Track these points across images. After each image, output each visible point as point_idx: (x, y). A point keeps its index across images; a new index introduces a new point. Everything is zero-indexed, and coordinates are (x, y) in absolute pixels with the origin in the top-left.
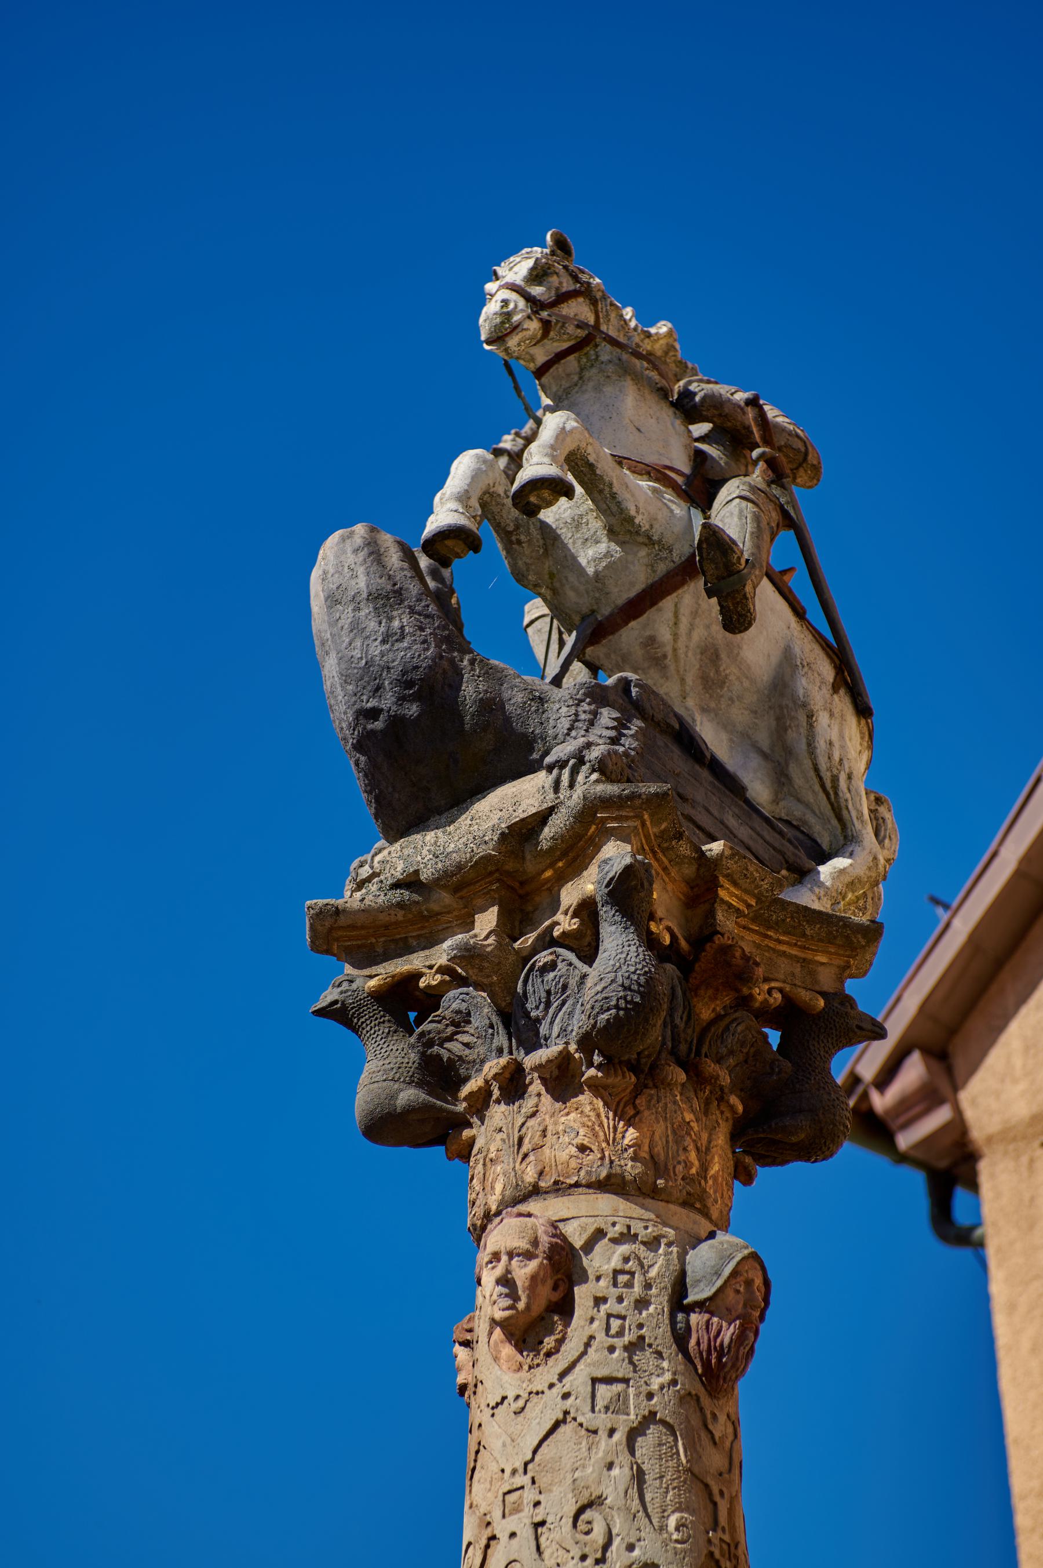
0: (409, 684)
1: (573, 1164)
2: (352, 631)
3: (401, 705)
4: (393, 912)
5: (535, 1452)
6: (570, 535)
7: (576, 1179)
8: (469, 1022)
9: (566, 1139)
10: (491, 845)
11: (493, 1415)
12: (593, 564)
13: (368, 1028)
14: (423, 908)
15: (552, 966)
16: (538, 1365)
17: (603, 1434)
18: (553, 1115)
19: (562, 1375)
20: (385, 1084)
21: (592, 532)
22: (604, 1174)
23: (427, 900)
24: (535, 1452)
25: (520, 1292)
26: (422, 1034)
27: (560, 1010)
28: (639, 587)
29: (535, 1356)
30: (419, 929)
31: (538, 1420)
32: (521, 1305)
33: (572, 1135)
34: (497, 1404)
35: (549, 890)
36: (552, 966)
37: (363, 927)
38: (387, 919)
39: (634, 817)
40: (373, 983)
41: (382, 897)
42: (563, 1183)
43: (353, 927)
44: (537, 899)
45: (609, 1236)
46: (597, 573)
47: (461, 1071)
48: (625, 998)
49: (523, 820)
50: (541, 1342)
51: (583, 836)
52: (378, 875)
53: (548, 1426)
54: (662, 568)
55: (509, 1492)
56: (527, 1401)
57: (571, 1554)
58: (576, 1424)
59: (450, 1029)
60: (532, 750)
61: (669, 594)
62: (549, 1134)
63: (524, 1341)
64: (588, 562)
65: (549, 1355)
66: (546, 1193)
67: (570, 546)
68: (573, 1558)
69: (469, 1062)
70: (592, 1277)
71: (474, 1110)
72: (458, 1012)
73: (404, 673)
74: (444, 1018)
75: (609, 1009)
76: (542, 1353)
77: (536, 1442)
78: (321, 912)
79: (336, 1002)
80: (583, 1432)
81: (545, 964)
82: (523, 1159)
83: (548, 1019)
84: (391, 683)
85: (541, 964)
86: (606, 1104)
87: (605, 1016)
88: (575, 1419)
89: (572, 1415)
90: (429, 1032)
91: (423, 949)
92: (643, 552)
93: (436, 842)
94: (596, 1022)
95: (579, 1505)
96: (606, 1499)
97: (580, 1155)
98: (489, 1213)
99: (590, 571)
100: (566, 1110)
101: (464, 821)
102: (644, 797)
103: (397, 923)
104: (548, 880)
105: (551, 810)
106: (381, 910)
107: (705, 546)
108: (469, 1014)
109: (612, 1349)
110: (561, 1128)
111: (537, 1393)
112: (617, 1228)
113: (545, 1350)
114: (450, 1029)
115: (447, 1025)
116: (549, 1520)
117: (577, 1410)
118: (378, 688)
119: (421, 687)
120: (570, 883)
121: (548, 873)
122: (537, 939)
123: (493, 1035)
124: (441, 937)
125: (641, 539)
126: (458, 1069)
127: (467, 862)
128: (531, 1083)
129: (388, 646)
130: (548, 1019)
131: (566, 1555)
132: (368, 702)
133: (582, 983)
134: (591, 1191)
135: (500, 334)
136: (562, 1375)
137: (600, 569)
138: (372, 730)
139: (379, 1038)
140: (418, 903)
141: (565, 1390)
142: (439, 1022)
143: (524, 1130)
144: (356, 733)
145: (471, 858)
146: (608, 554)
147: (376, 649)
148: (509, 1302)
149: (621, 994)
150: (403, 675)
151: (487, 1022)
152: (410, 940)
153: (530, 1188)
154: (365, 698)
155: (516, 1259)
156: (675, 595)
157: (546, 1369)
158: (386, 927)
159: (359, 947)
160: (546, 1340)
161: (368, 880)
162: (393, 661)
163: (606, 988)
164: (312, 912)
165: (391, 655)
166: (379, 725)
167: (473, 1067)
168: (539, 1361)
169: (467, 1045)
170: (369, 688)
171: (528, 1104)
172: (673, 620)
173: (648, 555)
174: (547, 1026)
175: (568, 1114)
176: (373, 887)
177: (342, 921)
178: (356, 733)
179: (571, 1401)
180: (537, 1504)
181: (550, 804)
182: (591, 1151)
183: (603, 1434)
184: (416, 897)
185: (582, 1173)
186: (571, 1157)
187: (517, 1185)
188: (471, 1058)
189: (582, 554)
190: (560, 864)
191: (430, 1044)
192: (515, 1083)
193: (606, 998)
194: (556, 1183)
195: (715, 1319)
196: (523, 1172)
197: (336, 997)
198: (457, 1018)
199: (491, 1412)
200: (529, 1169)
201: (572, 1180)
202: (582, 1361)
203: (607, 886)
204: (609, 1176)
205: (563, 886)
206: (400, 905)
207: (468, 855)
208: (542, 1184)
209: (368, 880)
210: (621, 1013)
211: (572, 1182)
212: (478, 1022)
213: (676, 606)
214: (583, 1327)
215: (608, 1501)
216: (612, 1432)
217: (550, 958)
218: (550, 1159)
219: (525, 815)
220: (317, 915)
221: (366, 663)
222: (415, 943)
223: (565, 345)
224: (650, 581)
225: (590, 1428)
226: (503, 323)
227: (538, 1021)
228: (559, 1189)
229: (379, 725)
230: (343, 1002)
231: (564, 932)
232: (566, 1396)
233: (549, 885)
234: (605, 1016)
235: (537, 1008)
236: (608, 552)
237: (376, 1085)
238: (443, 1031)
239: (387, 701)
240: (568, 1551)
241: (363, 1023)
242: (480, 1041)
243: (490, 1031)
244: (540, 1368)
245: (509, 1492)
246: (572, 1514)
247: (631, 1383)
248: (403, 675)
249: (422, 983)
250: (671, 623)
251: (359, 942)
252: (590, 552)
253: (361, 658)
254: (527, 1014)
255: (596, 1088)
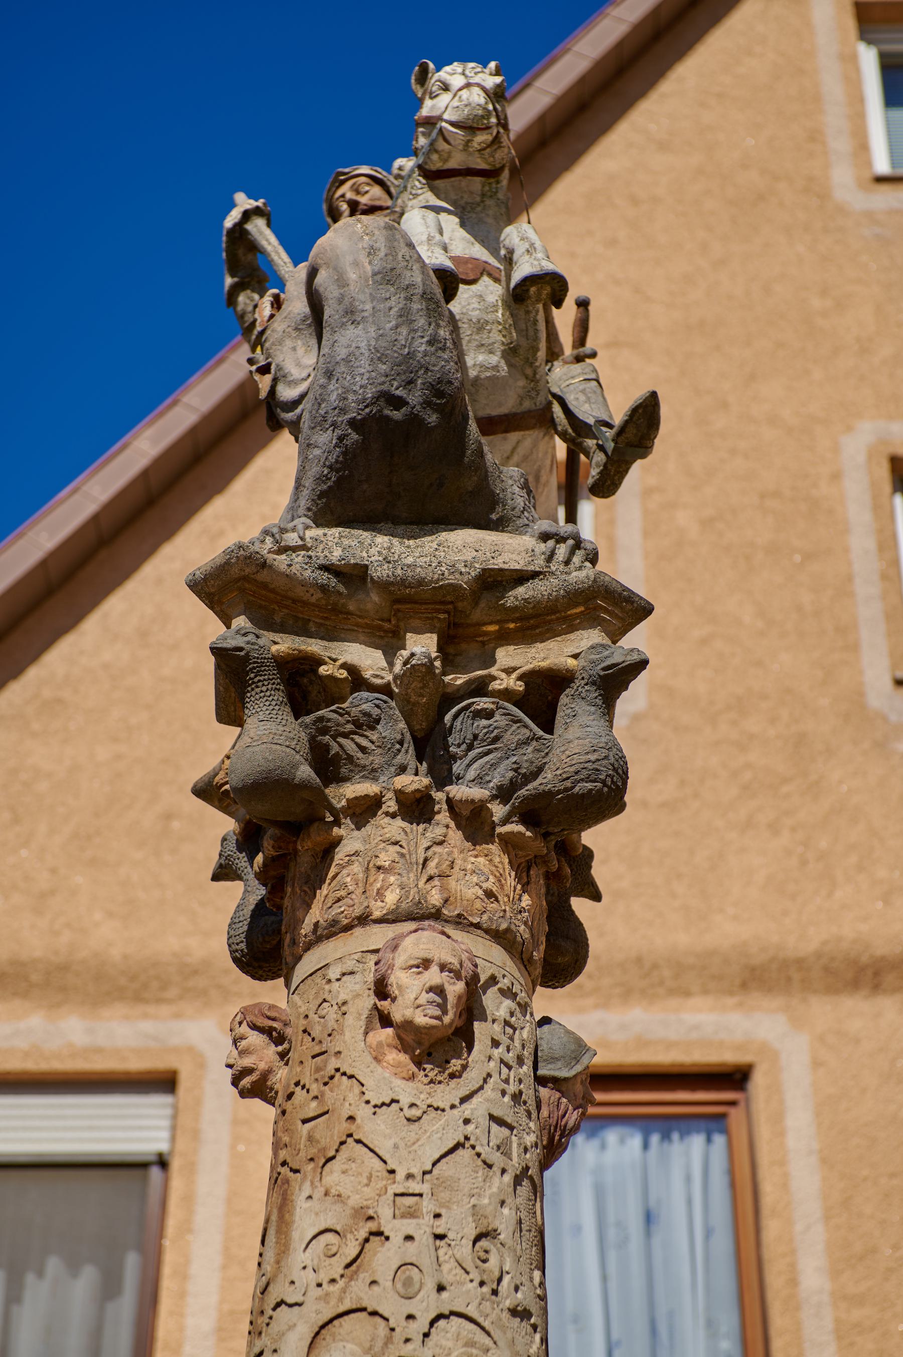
0: (440, 394)
1: (478, 905)
2: (401, 316)
3: (424, 408)
4: (312, 591)
5: (434, 1165)
6: (469, 333)
7: (478, 920)
8: (373, 728)
9: (475, 879)
10: (466, 578)
11: (374, 1113)
12: (478, 369)
13: (264, 688)
14: (344, 601)
15: (489, 715)
16: (440, 1082)
17: (496, 1170)
18: (462, 852)
19: (464, 1100)
20: (288, 750)
21: (491, 341)
22: (504, 926)
23: (350, 596)
24: (434, 1165)
25: (449, 1007)
26: (321, 719)
27: (482, 757)
28: (503, 410)
29: (440, 1072)
30: (323, 618)
31: (439, 1135)
32: (447, 1019)
33: (482, 878)
34: (383, 1104)
35: (483, 643)
36: (489, 715)
37: (273, 591)
38: (302, 594)
39: (622, 618)
40: (274, 648)
41: (309, 571)
42: (465, 918)
43: (264, 586)
44: (464, 646)
45: (499, 985)
46: (477, 378)
47: (343, 770)
48: (612, 777)
49: (501, 570)
50: (448, 1062)
51: (559, 612)
52: (308, 549)
53: (451, 1145)
54: (527, 405)
55: (402, 1195)
56: (424, 1112)
57: (471, 1276)
58: (473, 1152)
59: (350, 727)
60: (493, 510)
61: (520, 430)
62: (457, 868)
63: (429, 1054)
64: (474, 365)
65: (452, 1076)
66: (446, 921)
67: (464, 342)
68: (472, 1281)
69: (358, 765)
70: (490, 1019)
71: (350, 812)
72: (367, 714)
73: (440, 381)
74: (348, 713)
75: (595, 781)
76: (447, 1072)
77: (437, 1156)
78: (250, 557)
79: (241, 649)
80: (479, 1162)
81: (482, 710)
82: (428, 880)
83: (467, 761)
84: (424, 384)
85: (479, 707)
86: (510, 862)
87: (589, 785)
88: (473, 1147)
89: (472, 1142)
90: (329, 720)
91: (322, 638)
92: (522, 383)
93: (389, 548)
94: (573, 787)
95: (478, 1231)
96: (499, 1234)
97: (486, 900)
98: (368, 916)
99: (472, 373)
100: (475, 853)
101: (429, 543)
102: (635, 605)
103: (305, 603)
104: (486, 634)
105: (535, 575)
106: (303, 583)
107: (640, 411)
108: (378, 721)
109: (504, 1093)
110: (469, 866)
111: (437, 1109)
112: (506, 981)
113: (451, 1070)
114: (350, 727)
115: (348, 722)
116: (451, 1235)
117: (477, 1139)
118: (410, 382)
119: (448, 402)
120: (512, 647)
121: (492, 628)
122: (468, 683)
123: (399, 751)
124: (342, 635)
125: (529, 371)
126: (341, 767)
127: (431, 582)
128: (439, 812)
129: (433, 349)
130: (467, 761)
131: (465, 1275)
132: (397, 389)
133: (525, 743)
134: (487, 937)
135: (475, 125)
136: (464, 1100)
137: (483, 376)
138: (387, 417)
139: (274, 703)
140: (340, 594)
141: (467, 1114)
142: (341, 715)
143: (430, 853)
144: (367, 410)
145: (438, 580)
146: (496, 368)
147: (421, 347)
148: (438, 1012)
149: (610, 772)
150: (439, 383)
151: (399, 737)
152: (311, 624)
153: (433, 911)
154: (396, 384)
155: (447, 973)
156: (522, 433)
157: (447, 1088)
158: (294, 601)
159: (261, 607)
160: (453, 1061)
161: (294, 549)
162: (434, 365)
163: (598, 760)
164: (242, 552)
165: (433, 359)
166: (397, 415)
167: (360, 771)
168: (442, 1079)
169: (363, 749)
170: (403, 377)
171: (435, 832)
172: (508, 453)
173: (524, 387)
174: (463, 766)
175: (476, 856)
176: (299, 558)
177: (263, 576)
178: (367, 410)
179: (470, 1128)
180: (437, 1216)
181: (538, 569)
182: (497, 900)
183: (496, 1170)
184: (341, 588)
185: (485, 917)
186: (478, 897)
187: (420, 902)
188: (362, 762)
189: (472, 355)
190: (512, 626)
191: (324, 731)
192: (422, 805)
193: (597, 770)
194: (459, 916)
195: (564, 1100)
196: (427, 893)
197: (243, 645)
198: (363, 719)
199: (373, 1110)
200: (434, 891)
201: (476, 920)
202: (479, 1094)
203: (604, 669)
204: (508, 930)
205: (502, 646)
206: (323, 588)
207: (436, 576)
208: (445, 911)
209: (294, 549)
210: (606, 789)
211: (475, 922)
212: (384, 731)
213: (518, 442)
214: (483, 1062)
215: (502, 1237)
216: (504, 1171)
217: (492, 706)
218: (456, 891)
219: (506, 567)
220: (246, 558)
221: (408, 354)
222: (313, 629)
223: (483, 166)
224: (514, 410)
225: (488, 1161)
226: (483, 117)
227: (454, 758)
228: (460, 923)
229: (397, 415)
230: (247, 654)
231: (506, 689)
232: (467, 1121)
233: (485, 639)
234: (589, 785)
235: (459, 746)
236: (497, 366)
237: (278, 747)
238: (342, 725)
239: (415, 398)
240: (468, 1273)
241: (259, 681)
242: (379, 751)
243: (398, 746)
244: (442, 1086)
245: (402, 1195)
246: (472, 1238)
247: (515, 1132)
248: (439, 383)
249: (323, 670)
250: (505, 455)
251: (263, 603)
252: (481, 358)
253: (405, 346)
254: (446, 747)
255: (509, 843)
